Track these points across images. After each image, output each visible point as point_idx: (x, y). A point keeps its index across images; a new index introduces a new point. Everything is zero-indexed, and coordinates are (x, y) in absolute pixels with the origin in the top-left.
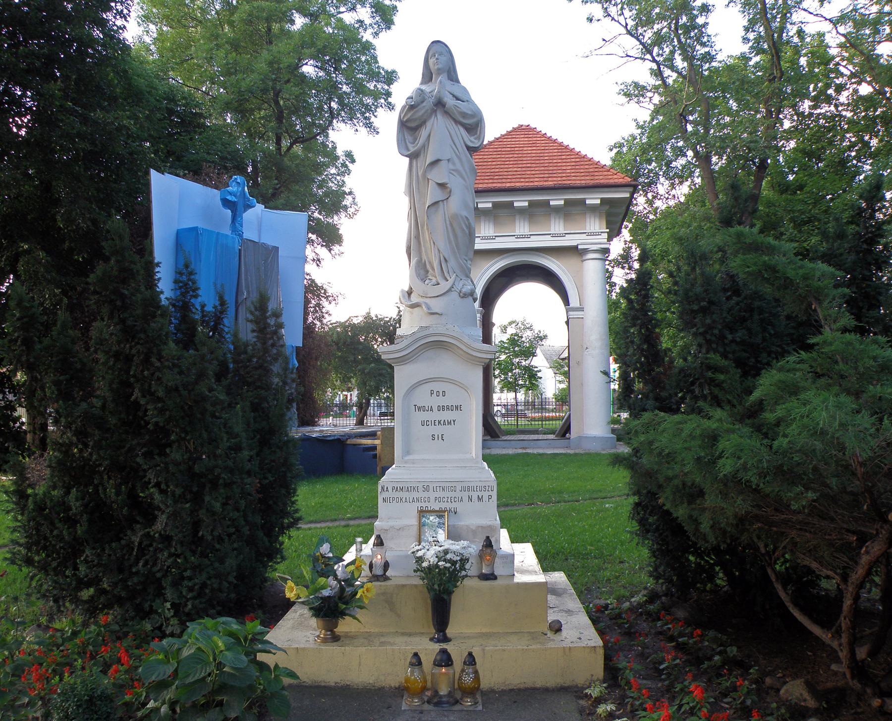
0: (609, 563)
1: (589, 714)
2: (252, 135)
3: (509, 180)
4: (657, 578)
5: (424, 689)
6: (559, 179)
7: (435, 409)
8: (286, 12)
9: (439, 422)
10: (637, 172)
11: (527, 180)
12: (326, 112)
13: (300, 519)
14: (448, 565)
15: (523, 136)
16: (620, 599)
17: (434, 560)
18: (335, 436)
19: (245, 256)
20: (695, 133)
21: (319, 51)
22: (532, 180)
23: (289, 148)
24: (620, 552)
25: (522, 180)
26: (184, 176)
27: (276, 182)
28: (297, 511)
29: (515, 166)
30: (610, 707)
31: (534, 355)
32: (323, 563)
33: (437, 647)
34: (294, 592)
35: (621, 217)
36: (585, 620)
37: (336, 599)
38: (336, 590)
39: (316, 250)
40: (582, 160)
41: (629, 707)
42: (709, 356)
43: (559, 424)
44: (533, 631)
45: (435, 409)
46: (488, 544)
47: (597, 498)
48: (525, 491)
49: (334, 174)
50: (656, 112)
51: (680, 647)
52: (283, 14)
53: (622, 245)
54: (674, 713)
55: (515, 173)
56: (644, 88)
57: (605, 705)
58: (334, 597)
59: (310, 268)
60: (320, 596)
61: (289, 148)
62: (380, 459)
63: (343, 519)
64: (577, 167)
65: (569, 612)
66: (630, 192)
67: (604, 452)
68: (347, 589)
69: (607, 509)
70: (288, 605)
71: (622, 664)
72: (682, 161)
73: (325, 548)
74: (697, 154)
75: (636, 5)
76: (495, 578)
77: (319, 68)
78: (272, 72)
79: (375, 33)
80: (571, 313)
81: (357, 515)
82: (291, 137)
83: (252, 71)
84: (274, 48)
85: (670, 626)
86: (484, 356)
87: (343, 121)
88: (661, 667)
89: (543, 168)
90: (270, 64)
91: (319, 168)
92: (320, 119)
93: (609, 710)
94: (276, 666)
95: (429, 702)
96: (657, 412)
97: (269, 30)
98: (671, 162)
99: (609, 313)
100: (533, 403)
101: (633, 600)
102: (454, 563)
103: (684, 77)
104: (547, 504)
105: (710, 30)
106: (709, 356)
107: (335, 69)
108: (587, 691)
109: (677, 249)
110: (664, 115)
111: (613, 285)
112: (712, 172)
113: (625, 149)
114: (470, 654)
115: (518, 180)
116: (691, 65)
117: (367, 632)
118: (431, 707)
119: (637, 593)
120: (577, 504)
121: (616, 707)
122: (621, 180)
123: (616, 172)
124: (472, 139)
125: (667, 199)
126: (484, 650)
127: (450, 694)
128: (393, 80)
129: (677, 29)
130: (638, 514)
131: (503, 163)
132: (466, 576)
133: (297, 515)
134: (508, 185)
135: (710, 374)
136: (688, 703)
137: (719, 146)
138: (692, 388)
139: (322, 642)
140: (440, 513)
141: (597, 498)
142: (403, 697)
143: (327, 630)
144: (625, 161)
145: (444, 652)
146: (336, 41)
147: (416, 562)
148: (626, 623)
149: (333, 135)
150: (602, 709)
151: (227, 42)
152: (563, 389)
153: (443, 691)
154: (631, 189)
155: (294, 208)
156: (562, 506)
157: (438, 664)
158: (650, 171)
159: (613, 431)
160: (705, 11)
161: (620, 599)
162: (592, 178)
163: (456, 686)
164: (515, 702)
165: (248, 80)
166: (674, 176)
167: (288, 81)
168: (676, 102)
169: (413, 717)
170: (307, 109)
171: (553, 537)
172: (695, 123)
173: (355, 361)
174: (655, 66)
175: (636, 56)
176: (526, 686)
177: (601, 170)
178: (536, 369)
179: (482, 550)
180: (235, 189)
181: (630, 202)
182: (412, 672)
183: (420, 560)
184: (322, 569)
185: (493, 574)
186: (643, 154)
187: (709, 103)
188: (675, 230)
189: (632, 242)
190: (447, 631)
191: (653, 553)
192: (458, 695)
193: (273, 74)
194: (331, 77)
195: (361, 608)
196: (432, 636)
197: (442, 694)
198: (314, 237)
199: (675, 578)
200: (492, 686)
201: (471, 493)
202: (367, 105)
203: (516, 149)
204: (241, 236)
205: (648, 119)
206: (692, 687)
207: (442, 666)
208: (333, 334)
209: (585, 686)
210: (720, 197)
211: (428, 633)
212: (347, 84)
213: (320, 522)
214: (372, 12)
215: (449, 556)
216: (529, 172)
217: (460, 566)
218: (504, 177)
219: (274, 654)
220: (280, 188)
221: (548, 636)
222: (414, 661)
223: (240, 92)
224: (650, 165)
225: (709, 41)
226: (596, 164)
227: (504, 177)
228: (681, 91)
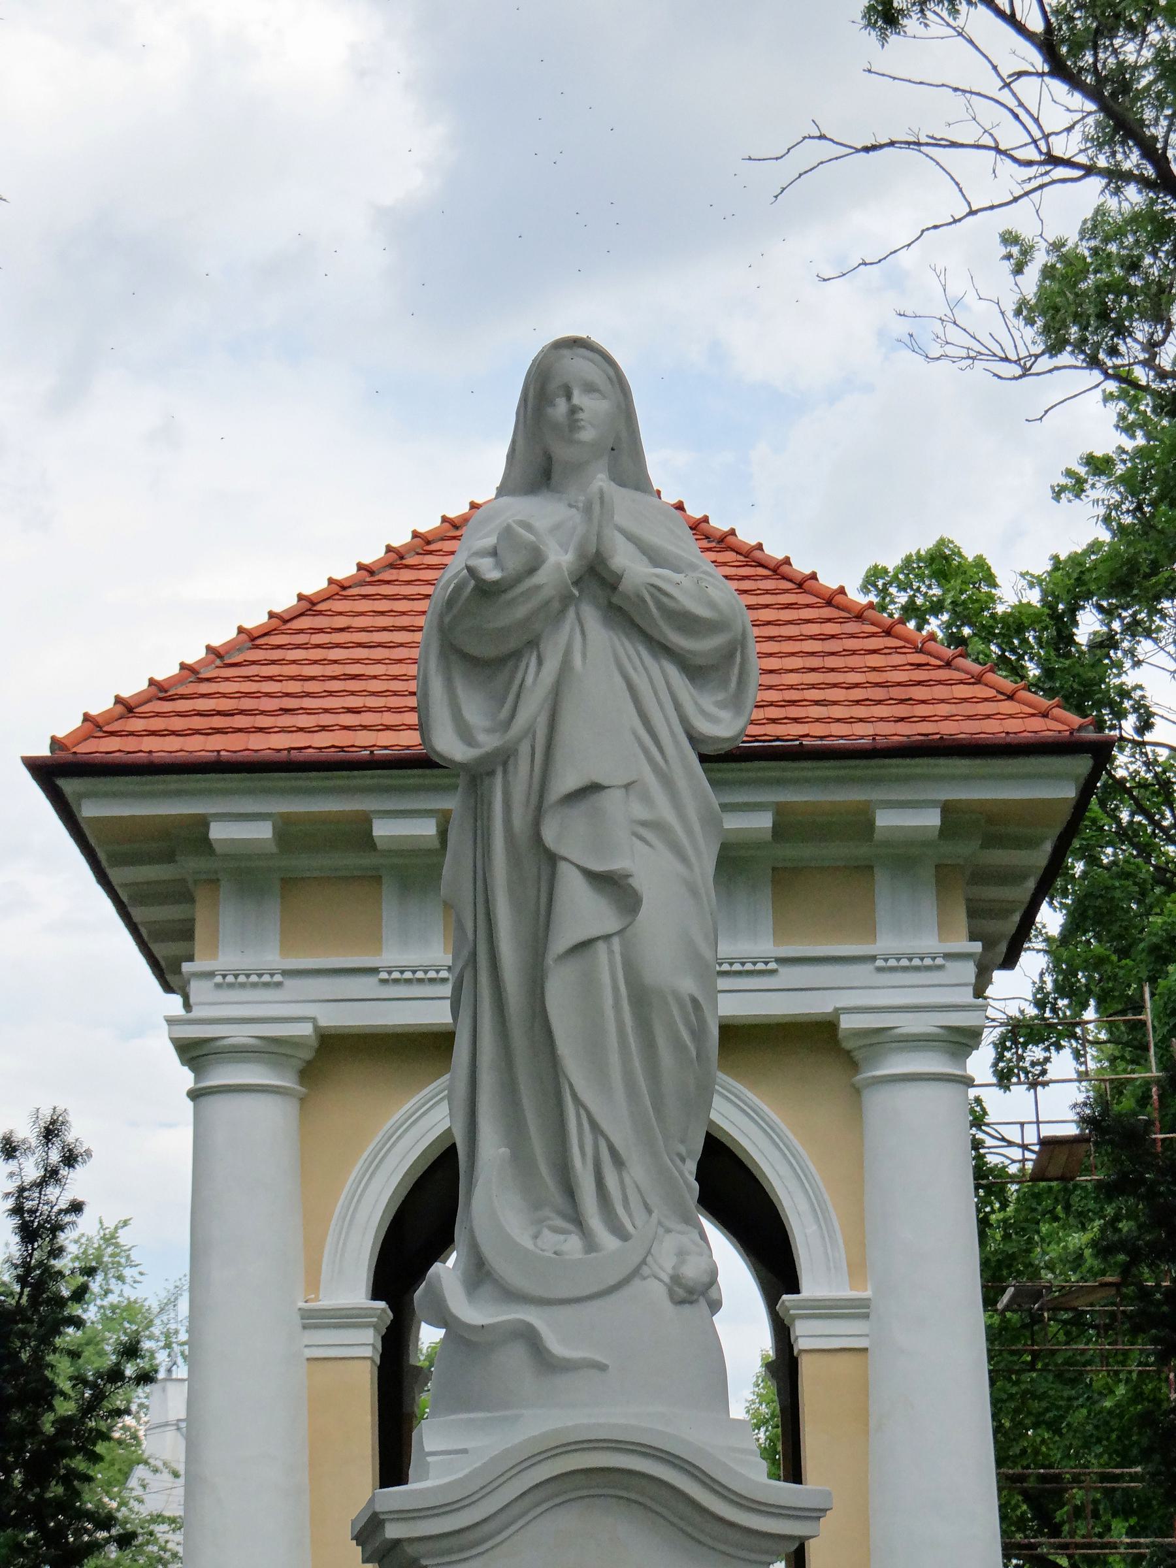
35: (1031, 884)
64: (831, 662)
122: (1037, 724)
124: (708, 702)
154: (1082, 765)
162: (902, 710)
226: (829, 603)
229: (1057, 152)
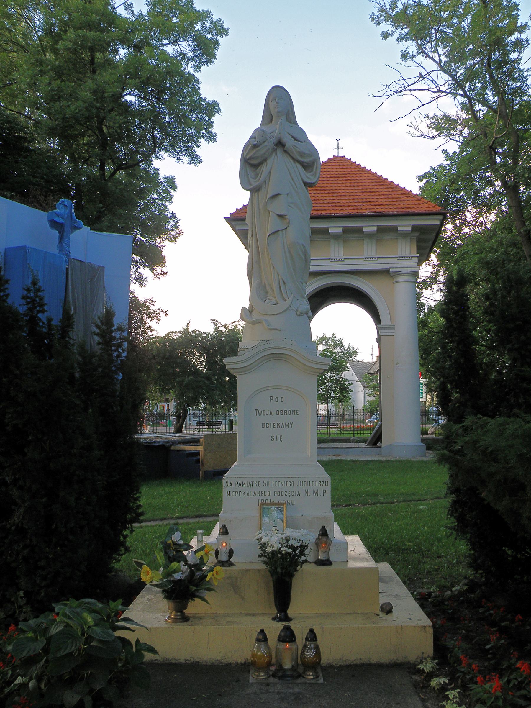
0: (427, 557)
1: (423, 688)
2: (76, 160)
3: (324, 208)
4: (476, 569)
5: (269, 664)
6: (372, 207)
7: (274, 413)
8: (109, 42)
9: (278, 425)
10: (446, 200)
11: (342, 208)
12: (149, 140)
13: (142, 514)
14: (290, 550)
15: (338, 167)
16: (442, 588)
17: (277, 546)
18: (159, 442)
19: (72, 274)
20: (504, 165)
21: (143, 82)
22: (346, 208)
23: (113, 174)
24: (438, 548)
25: (337, 208)
26: (12, 198)
27: (101, 205)
28: (139, 506)
29: (330, 195)
30: (443, 680)
31: (345, 369)
32: (174, 550)
33: (280, 626)
34: (150, 576)
35: (431, 243)
36: (414, 605)
37: (186, 582)
38: (187, 574)
39: (139, 270)
40: (394, 189)
41: (460, 681)
42: (523, 369)
43: (369, 435)
44: (366, 612)
45: (274, 413)
46: (324, 533)
47: (411, 501)
48: (342, 493)
49: (156, 199)
50: (464, 145)
51: (503, 631)
52: (107, 44)
53: (430, 269)
54: (504, 684)
55: (330, 201)
56: (454, 121)
57: (438, 679)
58: (184, 580)
59: (134, 287)
60: (172, 579)
61: (113, 174)
62: (203, 464)
63: (172, 518)
64: (390, 196)
65: (396, 596)
66: (440, 220)
67: (414, 460)
68: (197, 574)
69: (421, 511)
70: (140, 586)
71: (450, 643)
72: (490, 190)
73: (176, 537)
74: (505, 184)
75: (450, 42)
76: (330, 563)
77: (142, 98)
78: (96, 100)
79: (197, 65)
80: (381, 331)
81: (185, 515)
82: (114, 164)
83: (77, 99)
84: (98, 77)
85: (492, 612)
86: (315, 366)
87: (166, 149)
88: (488, 647)
89: (357, 197)
90: (95, 92)
91: (142, 193)
92: (144, 145)
93: (442, 682)
94: (138, 641)
95: (274, 676)
96: (479, 416)
97: (93, 59)
98: (479, 191)
99: (419, 331)
100: (343, 415)
101: (454, 589)
102: (294, 549)
103: (495, 111)
104: (364, 505)
105: (523, 66)
106: (523, 369)
107: (159, 99)
108: (419, 666)
109: (484, 273)
110: (474, 147)
111: (421, 305)
112: (519, 201)
113: (434, 179)
114: (312, 631)
115: (333, 208)
116: (502, 100)
117: (213, 613)
118: (276, 680)
119: (458, 583)
120: (392, 505)
121: (449, 680)
122: (432, 209)
123: (426, 201)
124: (309, 175)
125: (475, 225)
126: (323, 628)
127: (294, 668)
128: (214, 111)
129: (489, 65)
130: (457, 511)
131: (318, 192)
132: (306, 561)
133: (140, 511)
134: (324, 212)
135: (525, 385)
136: (516, 679)
137: (528, 177)
138: (508, 397)
139: (173, 622)
140: (279, 506)
141: (411, 501)
142: (249, 671)
143: (177, 611)
144: (434, 190)
145: (287, 629)
146: (160, 73)
147: (261, 548)
148: (450, 609)
149: (156, 163)
150: (435, 682)
151: (52, 70)
152: (372, 402)
153: (287, 665)
155: (118, 231)
156: (378, 507)
157: (282, 639)
158: (458, 200)
159: (423, 440)
160: (518, 46)
161: (442, 588)
162: (404, 206)
163: (299, 662)
164: (353, 676)
165: (73, 107)
166: (481, 204)
167: (112, 110)
168: (486, 135)
169: (260, 689)
170: (130, 136)
171: (373, 534)
172: (504, 155)
173: (174, 374)
174: (465, 100)
175: (448, 91)
176: (363, 662)
177: (413, 199)
178: (347, 383)
179: (318, 538)
180: (62, 211)
181: (439, 229)
182: (259, 649)
183: (263, 546)
184: (174, 555)
185: (328, 560)
186: (452, 184)
187: (518, 136)
188: (483, 255)
189: (439, 266)
190: (288, 612)
191: (473, 545)
192: (301, 670)
193: (98, 103)
194: (155, 108)
195: (209, 590)
196: (274, 616)
197: (286, 668)
198: (137, 258)
199: (493, 569)
200: (331, 662)
201: (307, 488)
202: (189, 135)
203: (332, 179)
204: (68, 255)
205: (458, 150)
206: (518, 665)
207: (286, 642)
208: (152, 349)
209: (416, 663)
210: (527, 224)
211: (269, 614)
212: (170, 115)
213: (150, 521)
214: (194, 46)
215: (290, 543)
216: (344, 201)
217: (300, 552)
218: (320, 205)
219: (134, 631)
220: (104, 211)
221: (380, 616)
222: (261, 637)
223: (64, 119)
224: (459, 194)
225: (520, 76)
226: (408, 194)
227: (320, 205)
228: (491, 124)
229: (441, 89)
